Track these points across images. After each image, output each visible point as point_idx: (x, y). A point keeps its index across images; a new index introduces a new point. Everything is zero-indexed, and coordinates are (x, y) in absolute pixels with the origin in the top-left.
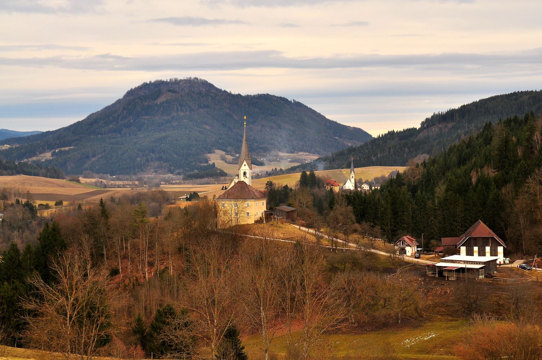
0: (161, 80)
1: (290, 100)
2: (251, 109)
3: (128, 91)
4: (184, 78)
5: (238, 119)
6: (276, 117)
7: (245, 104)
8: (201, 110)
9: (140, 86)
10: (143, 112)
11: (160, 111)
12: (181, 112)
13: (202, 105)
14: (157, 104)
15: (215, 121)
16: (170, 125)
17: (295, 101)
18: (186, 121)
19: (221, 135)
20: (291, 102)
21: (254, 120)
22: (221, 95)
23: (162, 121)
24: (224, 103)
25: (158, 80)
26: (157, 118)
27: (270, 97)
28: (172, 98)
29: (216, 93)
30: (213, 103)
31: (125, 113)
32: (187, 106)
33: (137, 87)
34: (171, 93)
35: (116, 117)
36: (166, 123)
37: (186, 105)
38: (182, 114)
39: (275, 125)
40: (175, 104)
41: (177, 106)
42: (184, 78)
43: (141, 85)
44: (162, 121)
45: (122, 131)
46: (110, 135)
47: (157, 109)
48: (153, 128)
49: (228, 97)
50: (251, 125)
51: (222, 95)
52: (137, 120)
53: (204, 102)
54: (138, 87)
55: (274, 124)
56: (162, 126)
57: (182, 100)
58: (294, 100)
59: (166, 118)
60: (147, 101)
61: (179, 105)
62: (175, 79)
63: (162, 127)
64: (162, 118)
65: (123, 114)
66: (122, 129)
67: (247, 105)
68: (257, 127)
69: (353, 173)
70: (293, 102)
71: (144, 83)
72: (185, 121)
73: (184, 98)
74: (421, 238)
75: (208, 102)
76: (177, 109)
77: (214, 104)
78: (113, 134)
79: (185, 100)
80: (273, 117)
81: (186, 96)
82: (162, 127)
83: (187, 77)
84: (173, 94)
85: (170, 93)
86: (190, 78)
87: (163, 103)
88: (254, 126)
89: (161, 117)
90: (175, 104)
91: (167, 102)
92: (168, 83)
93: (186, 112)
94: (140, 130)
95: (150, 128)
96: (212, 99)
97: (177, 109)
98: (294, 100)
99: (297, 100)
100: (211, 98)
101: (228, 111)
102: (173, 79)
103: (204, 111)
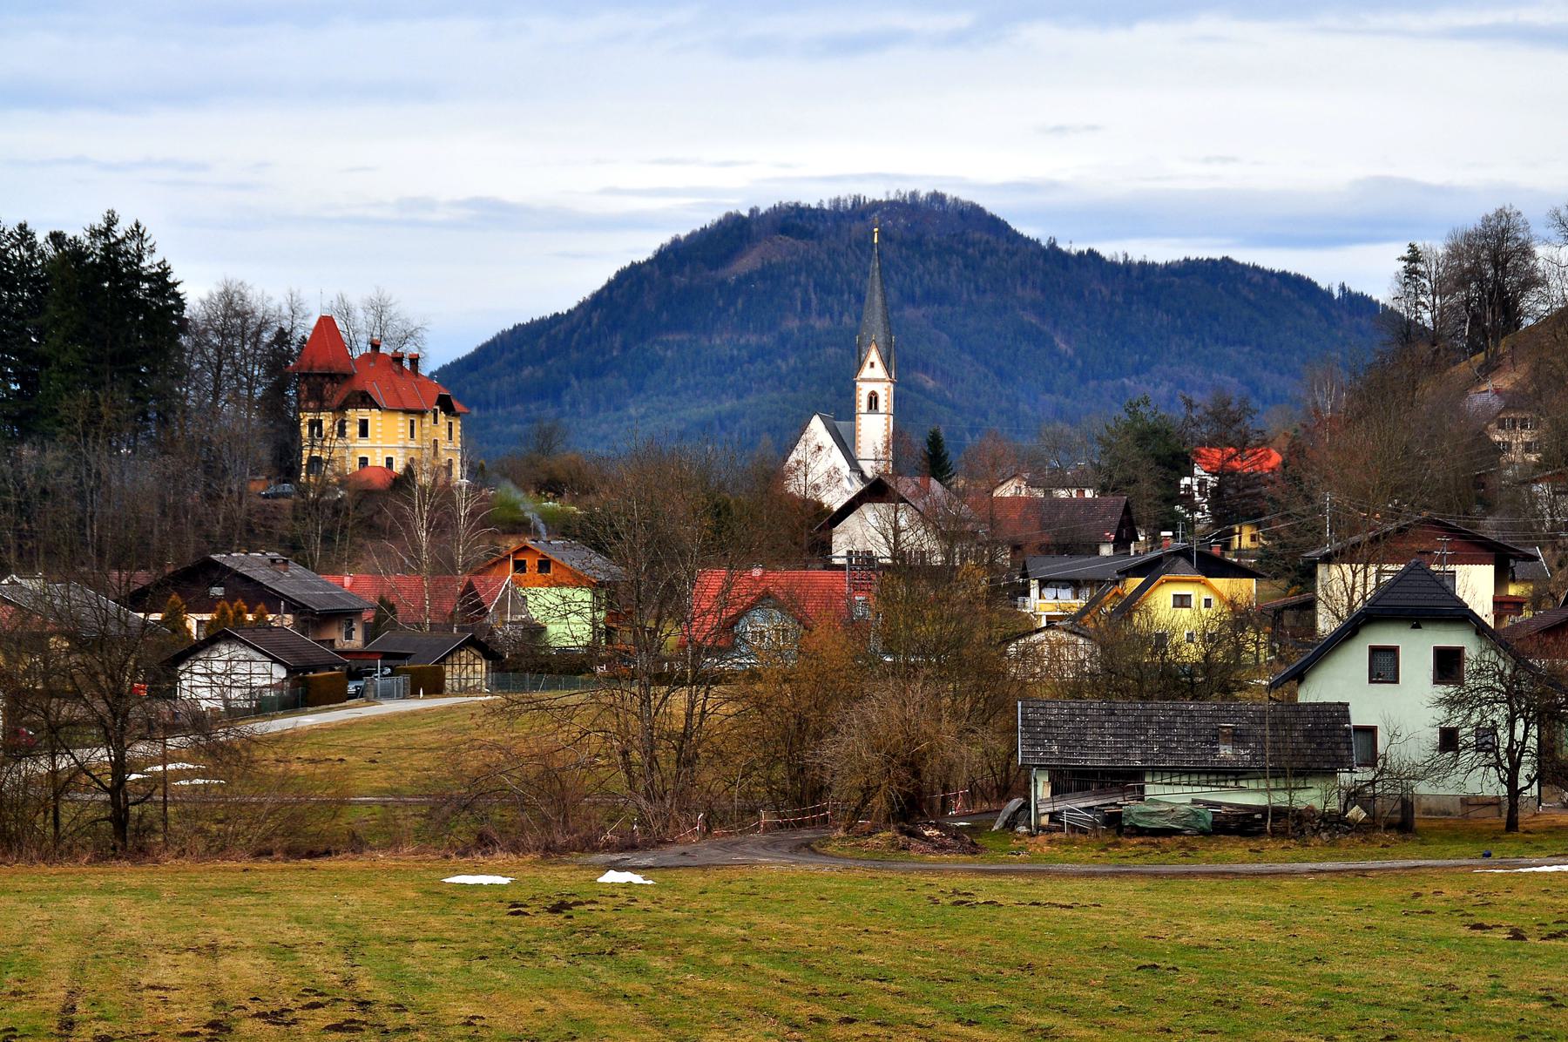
0: (797, 204)
1: (1323, 285)
2: (1138, 310)
3: (662, 246)
4: (888, 193)
5: (1070, 352)
6: (1247, 349)
7: (1113, 293)
8: (909, 312)
9: (711, 226)
10: (665, 314)
11: (732, 310)
12: (820, 314)
13: (918, 291)
14: (723, 283)
15: (968, 358)
16: (765, 366)
17: (1349, 291)
18: (836, 353)
19: (985, 415)
20: (1328, 294)
21: (1145, 358)
22: (1007, 250)
23: (735, 352)
24: (1018, 286)
25: (787, 206)
26: (718, 342)
27: (1232, 272)
28: (789, 259)
29: (988, 242)
30: (970, 282)
31: (595, 321)
32: (850, 293)
33: (698, 229)
34: (791, 240)
35: (561, 336)
36: (749, 363)
37: (845, 287)
38: (820, 324)
39: (1235, 380)
40: (797, 284)
41: (806, 291)
42: (888, 193)
43: (716, 221)
44: (735, 352)
45: (564, 392)
46: (518, 407)
47: (721, 303)
48: (692, 382)
49: (1041, 262)
50: (1126, 381)
51: (1014, 254)
52: (633, 350)
53: (928, 277)
54: (702, 229)
55: (1232, 376)
56: (733, 371)
57: (831, 265)
58: (1343, 288)
59: (753, 339)
60: (687, 270)
61: (815, 288)
62: (854, 200)
63: (732, 378)
64: (738, 340)
65: (589, 323)
66: (568, 385)
67: (1119, 299)
68: (1156, 386)
69: (879, 366)
70: (1336, 296)
71: (729, 217)
72: (831, 351)
73: (842, 261)
74: (463, 634)
75: (947, 281)
76: (806, 305)
77: (972, 286)
78: (532, 407)
79: (846, 268)
80: (1230, 350)
81: (850, 254)
82: (732, 378)
83: (898, 192)
84: (801, 245)
85: (787, 238)
86: (914, 195)
87: (749, 278)
88: (1140, 382)
89: (735, 337)
90: (797, 284)
91: (767, 273)
92: (823, 216)
93: (841, 314)
94: (640, 389)
95: (679, 382)
96: (966, 267)
97: (806, 305)
98: (1343, 288)
99: (1355, 288)
100: (960, 261)
101: (1030, 318)
102: (845, 201)
103: (923, 315)
